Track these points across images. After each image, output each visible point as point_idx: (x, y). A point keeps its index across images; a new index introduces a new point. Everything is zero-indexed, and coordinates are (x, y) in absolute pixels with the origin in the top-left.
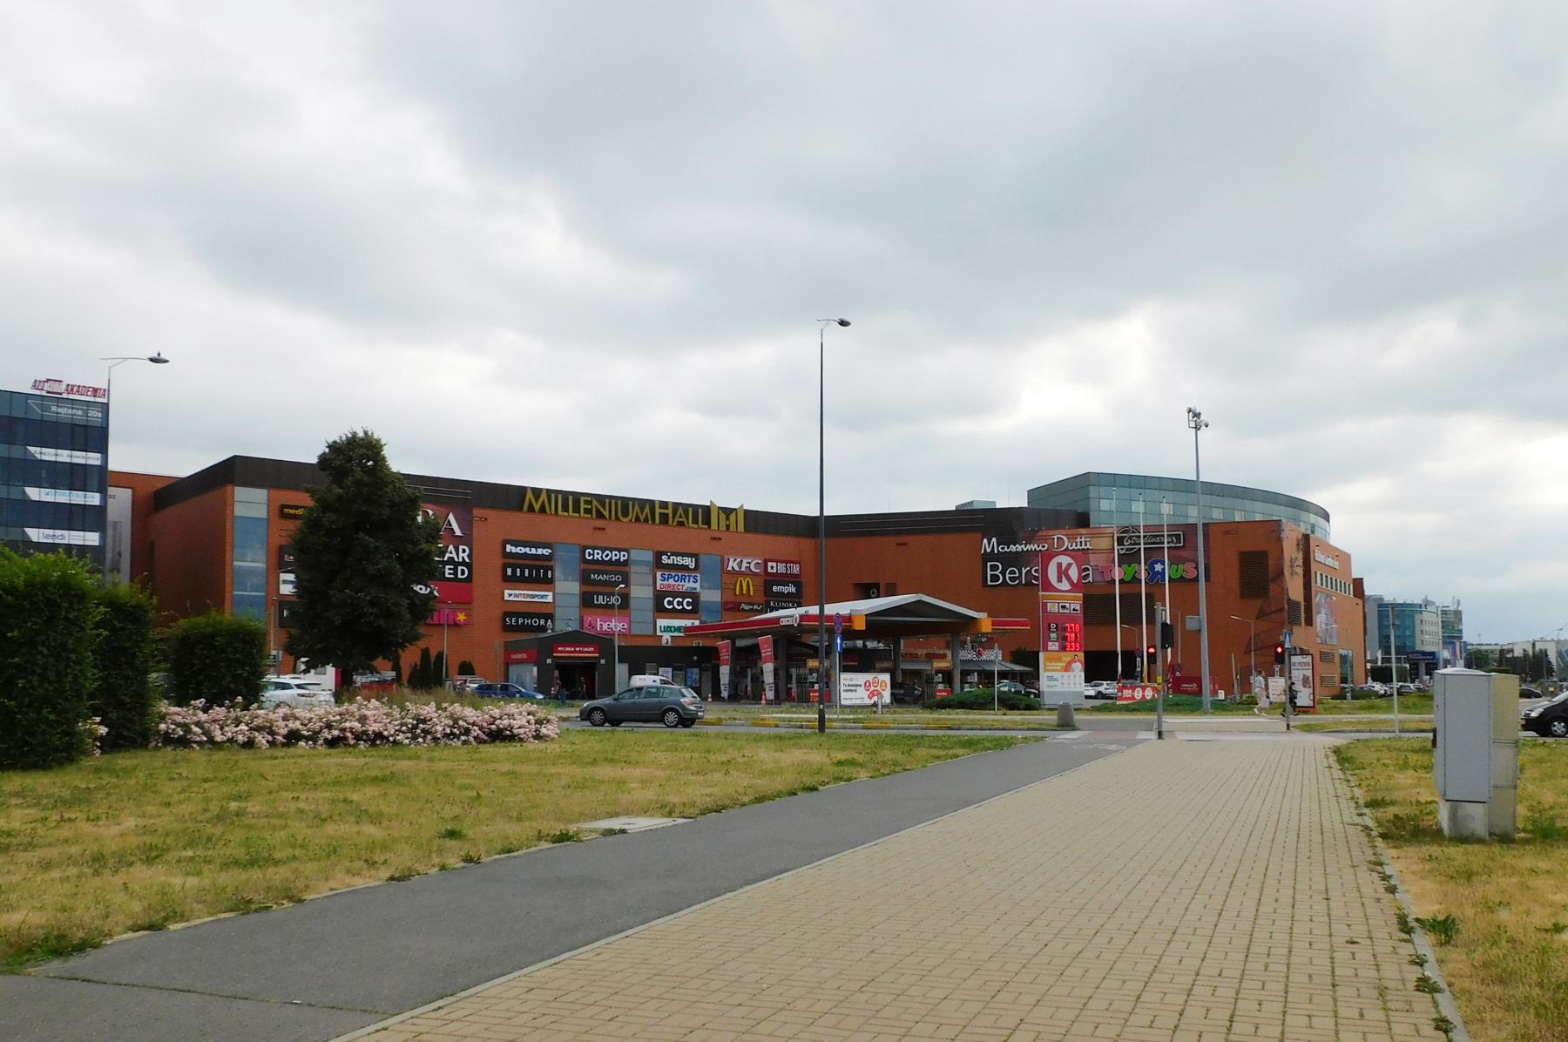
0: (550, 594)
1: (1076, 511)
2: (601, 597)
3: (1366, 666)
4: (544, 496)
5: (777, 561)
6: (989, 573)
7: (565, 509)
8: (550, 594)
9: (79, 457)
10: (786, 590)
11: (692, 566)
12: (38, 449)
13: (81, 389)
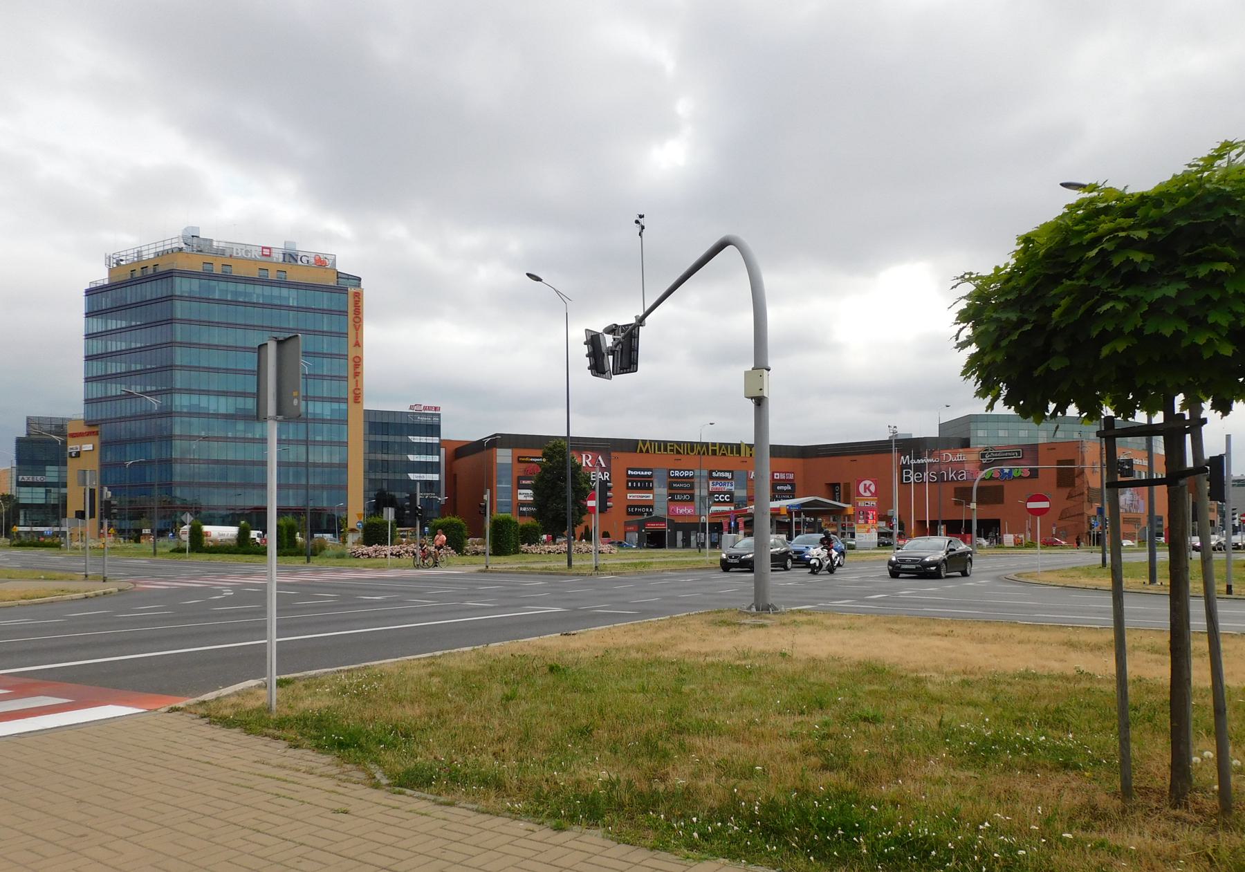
0: (651, 495)
1: (961, 438)
2: (678, 496)
3: (221, 549)
4: (648, 444)
5: (780, 473)
6: (904, 476)
7: (659, 450)
8: (651, 495)
9: (430, 440)
10: (785, 488)
11: (730, 477)
12: (412, 437)
13: (429, 408)
